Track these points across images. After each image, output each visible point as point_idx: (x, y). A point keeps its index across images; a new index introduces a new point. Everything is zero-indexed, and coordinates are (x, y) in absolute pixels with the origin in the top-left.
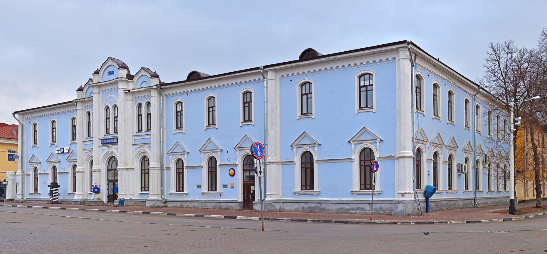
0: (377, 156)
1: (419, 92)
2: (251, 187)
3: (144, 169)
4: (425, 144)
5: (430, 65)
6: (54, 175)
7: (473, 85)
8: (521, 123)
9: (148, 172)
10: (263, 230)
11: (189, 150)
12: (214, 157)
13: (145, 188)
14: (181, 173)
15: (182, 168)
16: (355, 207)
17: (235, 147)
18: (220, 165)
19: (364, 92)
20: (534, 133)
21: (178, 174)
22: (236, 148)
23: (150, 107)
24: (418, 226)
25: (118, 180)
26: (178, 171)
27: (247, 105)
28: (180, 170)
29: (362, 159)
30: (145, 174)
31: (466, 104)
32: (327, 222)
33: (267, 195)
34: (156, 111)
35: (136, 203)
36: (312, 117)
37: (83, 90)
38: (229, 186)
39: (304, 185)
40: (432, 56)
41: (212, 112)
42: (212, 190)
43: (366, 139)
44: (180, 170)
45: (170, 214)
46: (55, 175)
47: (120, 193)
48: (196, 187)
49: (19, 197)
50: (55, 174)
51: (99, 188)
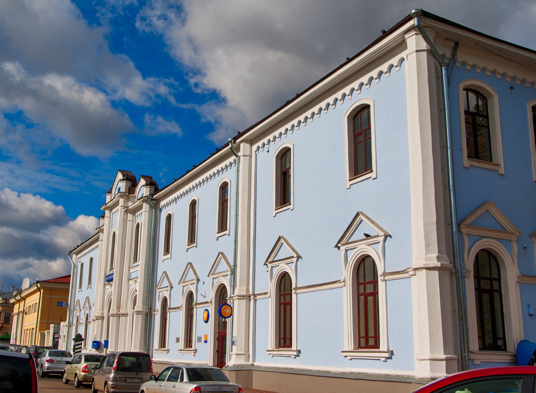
0: (50, 333)
1: (497, 277)
2: (372, 297)
3: (365, 284)
4: (231, 355)
5: (308, 373)
6: (362, 287)
7: (529, 117)
8: (101, 371)
9: (372, 291)
10: (457, 44)
11: (413, 50)
12: (370, 256)
13: (367, 337)
14: (370, 294)
15: (373, 280)
16: (125, 55)
17: (209, 275)
18: (385, 274)
19: (132, 278)
20: (177, 83)
21: (282, 306)
22: (210, 275)
23: (251, 302)
24: (168, 258)
25: (108, 341)
26: (362, 291)
27: (361, 138)
28: (367, 286)
29: (282, 293)
30: (366, 295)
31: (459, 235)
32: (465, 220)
33: (370, 339)
34: (479, 210)
35: (447, 31)
36: (498, 171)
37: (112, 192)
38: (203, 340)
39: (364, 336)
40: (356, 232)
41: (373, 339)
42: (367, 346)
43: (342, 377)
44: (367, 286)
45: (402, 24)
46: (494, 282)
47: (136, 317)
48: (176, 342)
49: (24, 345)
50: (284, 295)
51: (177, 382)
